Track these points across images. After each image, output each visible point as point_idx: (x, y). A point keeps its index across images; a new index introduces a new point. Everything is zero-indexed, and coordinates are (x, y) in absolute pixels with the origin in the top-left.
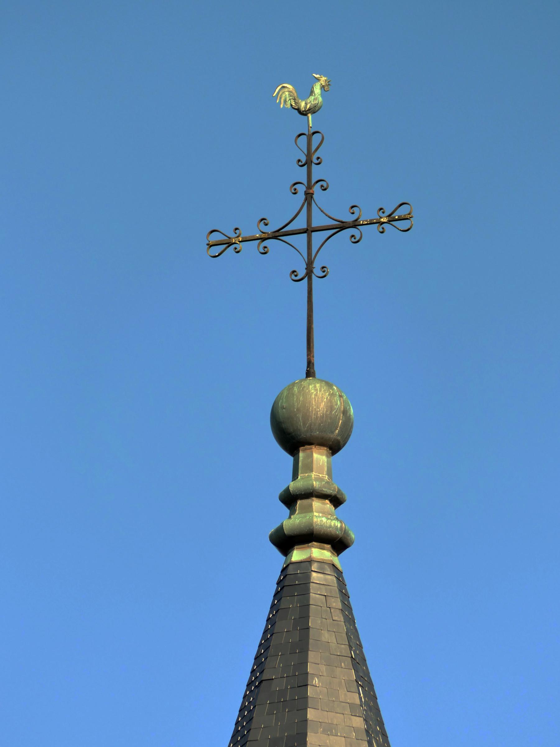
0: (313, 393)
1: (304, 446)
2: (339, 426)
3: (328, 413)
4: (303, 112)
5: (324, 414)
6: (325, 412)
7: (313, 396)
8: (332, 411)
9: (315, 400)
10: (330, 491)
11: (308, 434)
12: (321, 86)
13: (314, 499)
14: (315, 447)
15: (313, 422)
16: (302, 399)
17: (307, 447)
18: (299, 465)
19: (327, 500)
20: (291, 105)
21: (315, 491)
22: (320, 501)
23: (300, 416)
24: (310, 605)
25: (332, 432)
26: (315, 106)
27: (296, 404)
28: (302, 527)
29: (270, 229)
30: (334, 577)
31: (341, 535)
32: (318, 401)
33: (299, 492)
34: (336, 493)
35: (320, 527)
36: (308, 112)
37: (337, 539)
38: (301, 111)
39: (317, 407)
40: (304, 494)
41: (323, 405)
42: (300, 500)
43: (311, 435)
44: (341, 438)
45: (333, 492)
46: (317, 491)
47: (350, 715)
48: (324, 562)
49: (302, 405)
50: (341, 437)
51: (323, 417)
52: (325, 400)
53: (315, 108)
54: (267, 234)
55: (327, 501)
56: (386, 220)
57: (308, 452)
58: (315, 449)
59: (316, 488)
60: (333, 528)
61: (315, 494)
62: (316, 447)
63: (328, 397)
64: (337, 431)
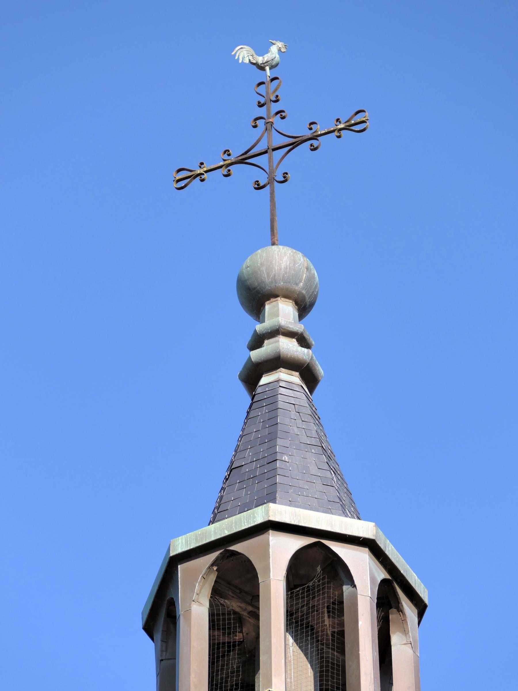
0: (276, 250)
1: (269, 299)
2: (304, 279)
4: (261, 65)
5: (287, 265)
6: (288, 264)
7: (276, 252)
8: (295, 264)
9: (278, 255)
10: (296, 328)
11: (273, 286)
12: (278, 47)
13: (281, 336)
14: (281, 299)
15: (277, 272)
16: (265, 255)
17: (272, 300)
18: (266, 315)
19: (294, 339)
20: (250, 60)
21: (281, 327)
22: (288, 339)
23: (264, 269)
25: (297, 284)
26: (273, 60)
27: (260, 260)
28: (269, 351)
29: (232, 159)
30: (303, 393)
31: (308, 361)
32: (281, 255)
33: (265, 330)
35: (286, 350)
36: (265, 65)
38: (259, 64)
39: (281, 260)
40: (270, 331)
41: (285, 259)
42: (267, 340)
43: (276, 286)
44: (306, 292)
45: (299, 330)
46: (283, 327)
47: (321, 484)
48: (293, 382)
49: (265, 259)
50: (306, 291)
51: (287, 268)
52: (288, 255)
53: (273, 61)
54: (230, 160)
56: (343, 126)
57: (274, 303)
58: (281, 300)
59: (282, 324)
60: (300, 352)
61: (281, 332)
62: (282, 299)
63: (290, 254)
64: (302, 283)
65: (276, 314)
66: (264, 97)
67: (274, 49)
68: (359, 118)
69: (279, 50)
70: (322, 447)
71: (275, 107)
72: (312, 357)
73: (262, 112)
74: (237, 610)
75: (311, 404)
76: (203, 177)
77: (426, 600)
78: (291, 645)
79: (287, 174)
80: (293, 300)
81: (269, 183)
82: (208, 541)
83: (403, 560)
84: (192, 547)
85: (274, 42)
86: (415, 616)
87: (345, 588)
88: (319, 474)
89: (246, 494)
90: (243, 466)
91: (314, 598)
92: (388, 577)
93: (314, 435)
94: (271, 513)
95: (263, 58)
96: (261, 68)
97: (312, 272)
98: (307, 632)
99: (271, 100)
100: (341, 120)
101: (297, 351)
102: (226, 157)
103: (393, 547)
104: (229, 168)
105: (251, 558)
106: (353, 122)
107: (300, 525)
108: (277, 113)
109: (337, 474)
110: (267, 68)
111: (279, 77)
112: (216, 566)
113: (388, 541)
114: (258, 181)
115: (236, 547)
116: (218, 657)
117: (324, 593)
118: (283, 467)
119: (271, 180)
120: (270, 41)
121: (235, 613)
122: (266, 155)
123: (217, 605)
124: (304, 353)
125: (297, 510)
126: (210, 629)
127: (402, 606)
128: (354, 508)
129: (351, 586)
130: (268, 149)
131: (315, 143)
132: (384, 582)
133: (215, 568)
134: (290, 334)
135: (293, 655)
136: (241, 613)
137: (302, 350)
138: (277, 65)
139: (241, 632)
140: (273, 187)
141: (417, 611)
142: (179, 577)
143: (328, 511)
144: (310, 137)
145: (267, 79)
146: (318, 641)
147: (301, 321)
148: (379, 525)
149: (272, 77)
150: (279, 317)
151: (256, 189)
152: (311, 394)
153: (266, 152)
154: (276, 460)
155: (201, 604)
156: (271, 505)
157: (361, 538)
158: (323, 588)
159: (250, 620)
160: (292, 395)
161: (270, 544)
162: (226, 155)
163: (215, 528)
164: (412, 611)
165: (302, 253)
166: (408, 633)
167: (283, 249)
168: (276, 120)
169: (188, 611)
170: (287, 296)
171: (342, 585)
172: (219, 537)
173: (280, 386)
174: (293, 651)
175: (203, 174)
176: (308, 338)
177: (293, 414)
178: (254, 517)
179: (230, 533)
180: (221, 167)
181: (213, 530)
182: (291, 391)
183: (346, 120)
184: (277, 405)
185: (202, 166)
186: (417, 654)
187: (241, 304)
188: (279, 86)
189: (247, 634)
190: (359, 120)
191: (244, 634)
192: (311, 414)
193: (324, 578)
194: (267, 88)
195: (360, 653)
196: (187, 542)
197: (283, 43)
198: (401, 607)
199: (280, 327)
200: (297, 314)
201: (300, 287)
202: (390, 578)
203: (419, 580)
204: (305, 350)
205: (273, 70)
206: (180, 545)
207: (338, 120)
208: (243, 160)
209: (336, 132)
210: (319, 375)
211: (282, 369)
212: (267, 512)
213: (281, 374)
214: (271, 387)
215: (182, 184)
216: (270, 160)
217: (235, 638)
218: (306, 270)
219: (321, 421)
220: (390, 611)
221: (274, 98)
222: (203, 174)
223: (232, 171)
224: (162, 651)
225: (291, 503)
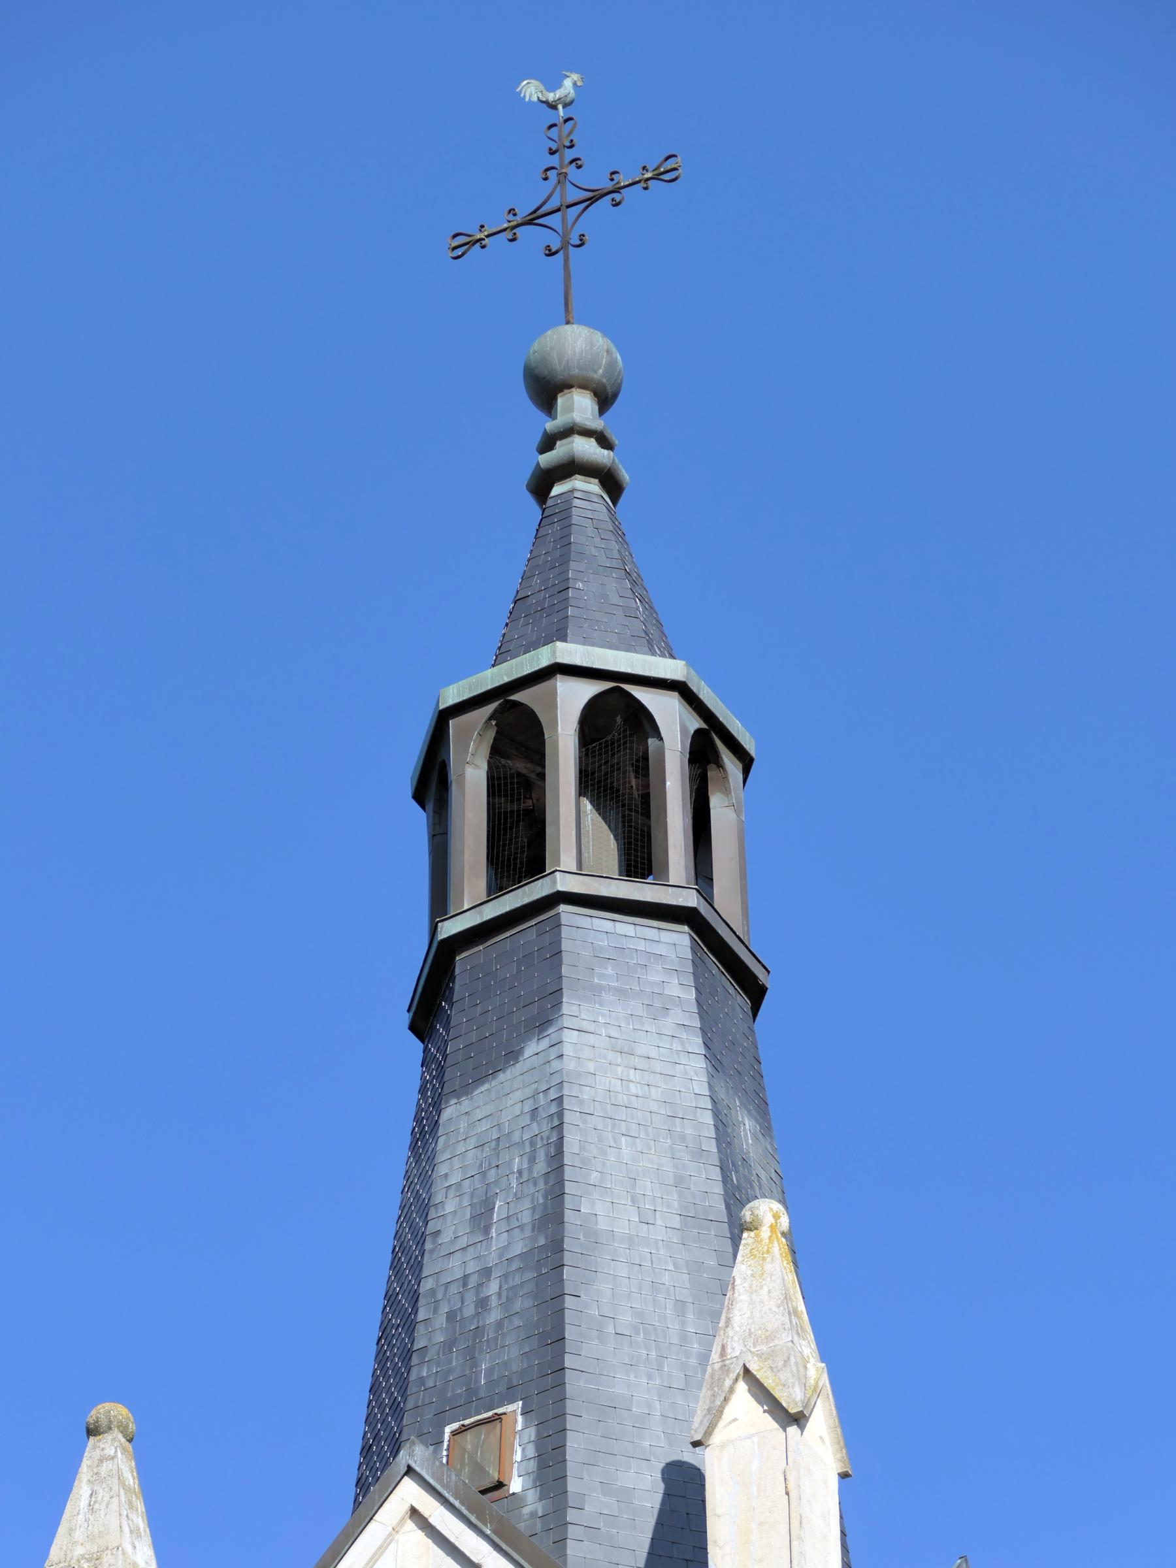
1: (562, 391)
3: (588, 348)
6: (584, 347)
7: (569, 333)
13: (576, 436)
17: (566, 391)
20: (538, 98)
23: (554, 354)
24: (564, 1265)
25: (595, 372)
26: (566, 96)
29: (519, 219)
31: (609, 465)
34: (601, 428)
36: (558, 102)
37: (604, 470)
52: (584, 335)
55: (593, 440)
65: (570, 409)
66: (556, 142)
67: (568, 83)
68: (670, 164)
69: (575, 84)
70: (626, 570)
71: (569, 155)
72: (614, 460)
73: (554, 160)
74: (524, 771)
75: (613, 519)
76: (484, 243)
77: (753, 753)
78: (589, 812)
79: (583, 235)
80: (591, 391)
81: (562, 248)
82: (484, 690)
83: (723, 705)
84: (465, 698)
85: (568, 74)
86: (738, 769)
87: (650, 741)
88: (621, 604)
89: (532, 631)
90: (529, 596)
91: (613, 755)
92: (704, 726)
93: (616, 555)
94: (558, 654)
95: (555, 94)
96: (553, 106)
97: (614, 356)
98: (605, 796)
99: (564, 146)
100: (648, 167)
101: (595, 454)
102: (511, 217)
103: (709, 690)
104: (514, 231)
105: (535, 710)
106: (662, 170)
107: (594, 667)
108: (572, 162)
109: (644, 603)
110: (560, 107)
111: (573, 117)
112: (494, 720)
113: (703, 682)
114: (549, 246)
115: (516, 697)
116: (505, 829)
117: (625, 749)
118: (576, 596)
119: (565, 244)
120: (563, 73)
121: (519, 775)
122: (559, 214)
123: (497, 767)
124: (604, 457)
125: (590, 648)
126: (488, 796)
127: (723, 760)
128: (666, 643)
129: (658, 738)
130: (562, 206)
131: (617, 197)
132: (698, 732)
133: (494, 723)
134: (587, 433)
135: (592, 824)
136: (527, 775)
137: (600, 452)
138: (571, 102)
139: (531, 798)
140: (568, 253)
141: (741, 765)
142: (451, 734)
143: (629, 648)
144: (611, 189)
145: (559, 120)
146: (624, 806)
147: (603, 416)
148: (690, 663)
149: (566, 117)
150: (573, 411)
151: (547, 255)
152: (615, 506)
153: (558, 210)
154: (568, 588)
155: (477, 767)
156: (558, 644)
157: (667, 680)
158: (625, 743)
159: (539, 783)
160: (590, 508)
161: (558, 691)
162: (511, 214)
163: (491, 674)
164: (735, 766)
165: (601, 332)
166: (730, 793)
167: (578, 328)
168: (571, 170)
169: (462, 776)
170: (583, 386)
171: (647, 739)
172: (497, 684)
173: (575, 497)
174: (592, 820)
175: (483, 239)
176: (610, 436)
177: (591, 531)
178: (538, 659)
179: (510, 680)
180: (505, 230)
181: (490, 676)
182: (588, 503)
183: (655, 167)
184: (571, 521)
185: (483, 230)
186: (741, 817)
187: (530, 398)
188: (574, 127)
189: (538, 800)
190: (669, 167)
191: (534, 800)
192: (612, 529)
193: (625, 731)
194: (560, 132)
195: (668, 820)
196: (459, 692)
197: (579, 75)
198: (721, 763)
199: (575, 424)
200: (596, 408)
201: (599, 374)
202: (706, 727)
203: (743, 729)
204: (606, 452)
205: (568, 108)
206: (451, 696)
207: (644, 168)
208: (532, 220)
209: (642, 182)
210: (623, 481)
211: (577, 476)
212: (554, 653)
213: (577, 482)
214: (564, 498)
215: (459, 252)
216: (564, 218)
217: (593, 782)
218: (606, 353)
219: (626, 538)
220: (708, 767)
221: (568, 144)
222: (483, 239)
223: (518, 234)
224: (434, 824)
225: (586, 641)
